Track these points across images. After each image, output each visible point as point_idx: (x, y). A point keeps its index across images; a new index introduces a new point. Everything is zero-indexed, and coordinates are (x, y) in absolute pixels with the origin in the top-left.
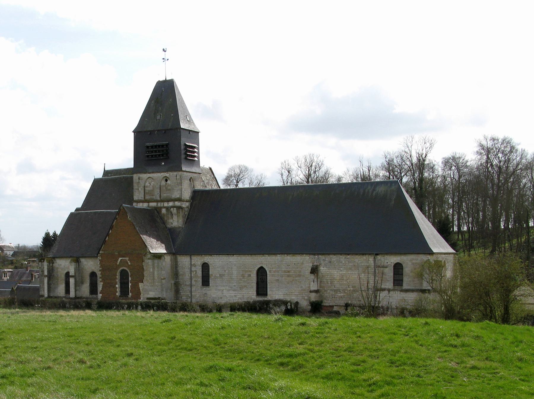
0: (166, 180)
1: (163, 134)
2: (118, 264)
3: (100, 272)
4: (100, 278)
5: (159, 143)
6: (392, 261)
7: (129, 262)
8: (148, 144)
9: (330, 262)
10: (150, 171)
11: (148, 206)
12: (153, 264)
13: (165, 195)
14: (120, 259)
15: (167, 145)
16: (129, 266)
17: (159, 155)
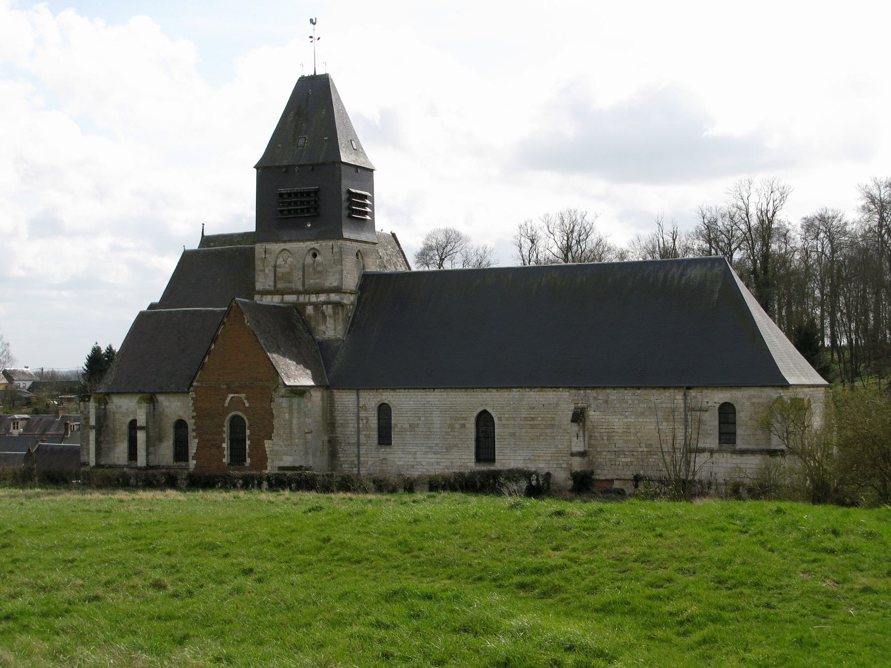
0: (315, 256)
1: (309, 169)
2: (226, 405)
7: (246, 401)
8: (282, 190)
9: (607, 402)
10: (285, 238)
11: (282, 302)
12: (290, 406)
13: (311, 281)
14: (230, 396)
15: (316, 192)
16: (245, 410)
17: (302, 210)
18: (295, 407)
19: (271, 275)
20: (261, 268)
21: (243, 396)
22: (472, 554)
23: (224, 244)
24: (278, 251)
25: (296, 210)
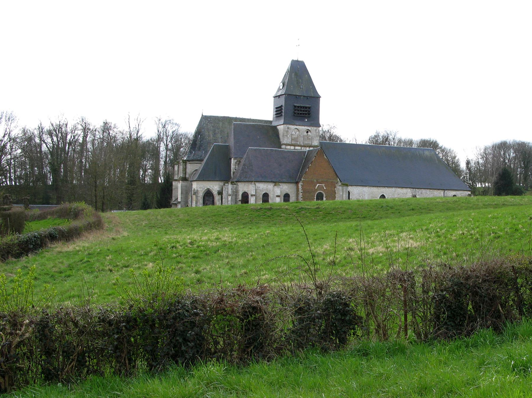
0: (307, 132)
1: (299, 99)
5: (304, 105)
8: (295, 105)
11: (295, 149)
12: (343, 190)
14: (318, 185)
15: (309, 108)
19: (290, 138)
25: (301, 114)
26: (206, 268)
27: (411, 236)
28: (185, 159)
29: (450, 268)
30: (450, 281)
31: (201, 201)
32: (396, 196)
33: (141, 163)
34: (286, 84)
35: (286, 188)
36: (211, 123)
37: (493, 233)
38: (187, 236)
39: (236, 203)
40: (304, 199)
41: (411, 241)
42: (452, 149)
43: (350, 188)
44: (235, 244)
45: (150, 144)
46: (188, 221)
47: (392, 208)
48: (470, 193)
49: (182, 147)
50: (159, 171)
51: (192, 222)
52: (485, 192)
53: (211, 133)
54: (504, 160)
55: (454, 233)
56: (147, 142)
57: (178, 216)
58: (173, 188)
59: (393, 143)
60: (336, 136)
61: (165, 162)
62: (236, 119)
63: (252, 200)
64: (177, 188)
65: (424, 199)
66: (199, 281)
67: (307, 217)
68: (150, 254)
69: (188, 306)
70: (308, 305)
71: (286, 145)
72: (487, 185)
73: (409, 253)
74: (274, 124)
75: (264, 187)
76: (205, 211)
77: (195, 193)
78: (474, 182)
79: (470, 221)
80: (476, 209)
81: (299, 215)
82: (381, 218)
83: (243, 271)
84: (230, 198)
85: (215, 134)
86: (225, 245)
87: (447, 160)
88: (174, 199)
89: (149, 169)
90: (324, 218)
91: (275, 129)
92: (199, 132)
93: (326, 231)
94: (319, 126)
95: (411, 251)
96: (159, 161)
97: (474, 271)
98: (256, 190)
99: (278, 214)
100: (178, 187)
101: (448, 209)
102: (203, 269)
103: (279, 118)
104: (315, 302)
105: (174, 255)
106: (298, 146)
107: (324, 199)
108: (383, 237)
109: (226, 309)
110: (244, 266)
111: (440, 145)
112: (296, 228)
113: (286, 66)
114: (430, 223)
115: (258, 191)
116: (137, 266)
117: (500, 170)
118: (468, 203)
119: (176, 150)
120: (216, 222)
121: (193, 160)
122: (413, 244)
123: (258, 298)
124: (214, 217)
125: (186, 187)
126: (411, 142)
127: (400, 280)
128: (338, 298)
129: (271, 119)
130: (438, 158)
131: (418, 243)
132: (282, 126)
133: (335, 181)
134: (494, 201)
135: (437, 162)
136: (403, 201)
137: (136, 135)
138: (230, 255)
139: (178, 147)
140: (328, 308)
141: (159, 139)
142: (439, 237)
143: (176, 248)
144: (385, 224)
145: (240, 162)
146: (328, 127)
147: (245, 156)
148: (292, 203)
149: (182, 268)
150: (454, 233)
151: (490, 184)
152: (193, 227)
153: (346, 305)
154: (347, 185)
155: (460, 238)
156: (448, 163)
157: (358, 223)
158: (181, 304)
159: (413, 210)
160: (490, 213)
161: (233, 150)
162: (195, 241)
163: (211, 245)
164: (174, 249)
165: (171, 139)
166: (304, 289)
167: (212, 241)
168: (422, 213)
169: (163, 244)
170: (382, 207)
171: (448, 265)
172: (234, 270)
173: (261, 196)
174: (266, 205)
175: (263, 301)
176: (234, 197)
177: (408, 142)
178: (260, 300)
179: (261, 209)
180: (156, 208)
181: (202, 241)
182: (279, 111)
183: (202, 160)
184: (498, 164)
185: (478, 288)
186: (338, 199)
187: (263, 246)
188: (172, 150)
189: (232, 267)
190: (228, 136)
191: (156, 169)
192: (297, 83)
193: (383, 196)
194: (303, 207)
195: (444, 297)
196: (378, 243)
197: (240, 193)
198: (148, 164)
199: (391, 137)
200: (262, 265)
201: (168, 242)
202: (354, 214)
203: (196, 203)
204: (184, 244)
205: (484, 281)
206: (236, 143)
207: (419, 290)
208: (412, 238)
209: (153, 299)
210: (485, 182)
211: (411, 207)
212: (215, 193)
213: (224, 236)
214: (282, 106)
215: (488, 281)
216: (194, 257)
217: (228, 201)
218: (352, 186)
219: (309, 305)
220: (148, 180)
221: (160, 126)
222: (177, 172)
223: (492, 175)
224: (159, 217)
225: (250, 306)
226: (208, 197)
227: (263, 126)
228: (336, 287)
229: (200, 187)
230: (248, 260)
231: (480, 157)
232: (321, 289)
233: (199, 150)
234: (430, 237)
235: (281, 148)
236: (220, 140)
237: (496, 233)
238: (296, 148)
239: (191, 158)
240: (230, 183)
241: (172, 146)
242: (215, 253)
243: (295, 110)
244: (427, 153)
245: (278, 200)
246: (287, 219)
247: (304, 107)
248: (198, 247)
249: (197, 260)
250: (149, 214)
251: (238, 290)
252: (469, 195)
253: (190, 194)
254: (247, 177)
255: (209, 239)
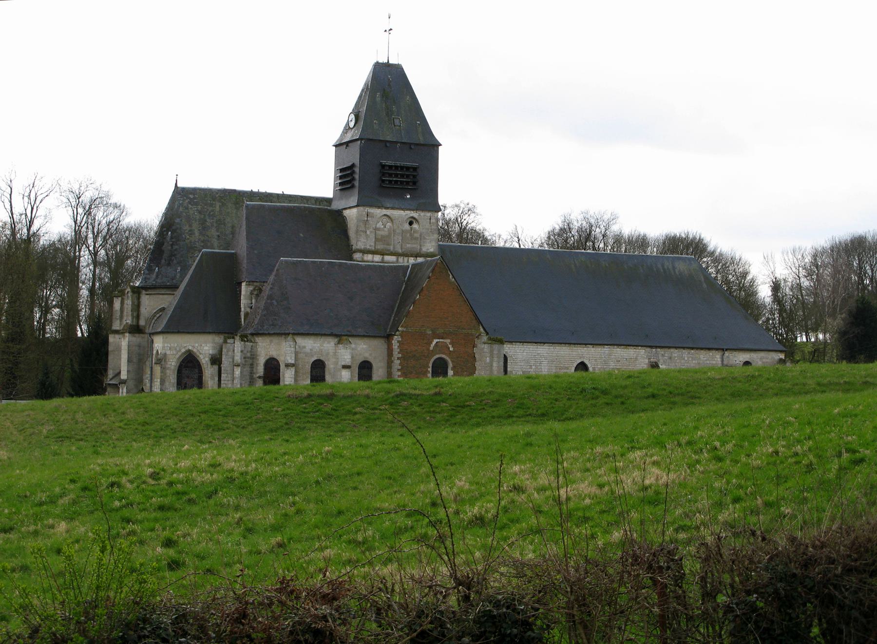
0: (411, 223)
1: (391, 145)
2: (431, 348)
3: (399, 362)
4: (398, 370)
5: (403, 164)
6: (741, 359)
7: (450, 346)
9: (670, 358)
10: (388, 206)
12: (491, 352)
13: (408, 246)
14: (435, 341)
15: (415, 169)
16: (450, 354)
17: (407, 183)
18: (495, 352)
20: (363, 229)
21: (448, 341)
22: (781, 466)
23: (290, 202)
24: (379, 216)
25: (396, 182)
26: (195, 534)
27: (655, 458)
28: (137, 284)
29: (764, 539)
30: (766, 569)
31: (172, 378)
32: (612, 365)
33: (36, 292)
34: (362, 115)
35: (363, 348)
36: (196, 204)
37: (847, 451)
38: (141, 460)
39: (252, 382)
40: (406, 372)
41: (655, 470)
42: (737, 257)
43: (509, 349)
44: (254, 478)
45: (57, 250)
46: (145, 423)
47: (605, 392)
48: (782, 356)
49: (129, 257)
50: (78, 311)
51: (154, 428)
52: (817, 354)
53: (196, 226)
54: (861, 280)
55: (754, 451)
56: (50, 245)
57: (123, 413)
58: (110, 348)
59: (602, 245)
60: (473, 231)
61: (92, 291)
62: (252, 195)
63: (288, 377)
64: (119, 349)
65: (679, 371)
66: (174, 565)
67: (414, 414)
68: (61, 502)
69: (166, 630)
70: (441, 626)
71: (365, 252)
72: (821, 336)
73: (654, 498)
74: (336, 206)
75: (314, 347)
76: (182, 402)
77: (159, 361)
78: (790, 330)
79: (788, 423)
80: (800, 393)
81: (400, 409)
82: (582, 416)
83: (273, 541)
84: (238, 372)
85: (204, 229)
86: (232, 480)
87: (727, 282)
88: (111, 373)
89: (55, 307)
90: (451, 416)
91: (338, 217)
92: (169, 222)
93: (459, 446)
94: (437, 209)
95: (657, 493)
96: (78, 289)
97: (823, 545)
98: (296, 353)
99: (348, 407)
100: (121, 347)
101: (736, 395)
102: (184, 536)
103: (347, 193)
104: (455, 618)
105: (117, 504)
106: (392, 254)
107: (450, 372)
108: (589, 460)
109: (254, 636)
110: (276, 528)
111: (711, 248)
112: (391, 440)
113: (358, 79)
114: (696, 428)
115: (301, 356)
116: (32, 528)
117: (852, 304)
118: (780, 381)
119: (115, 265)
120: (208, 426)
121: (154, 288)
122: (655, 477)
123: (325, 609)
124: (203, 416)
125: (139, 346)
126: (642, 242)
127: (650, 567)
128: (508, 608)
129: (329, 194)
130: (707, 276)
131: (672, 476)
132: (355, 210)
133: (473, 332)
134: (842, 376)
135: (705, 286)
136: (629, 377)
137: (25, 230)
138: (243, 503)
139: (121, 259)
140: (485, 632)
141: (78, 239)
142: (720, 459)
143: (119, 485)
144: (593, 432)
145: (260, 290)
146: (456, 209)
147: (272, 278)
148: (379, 383)
149: (133, 533)
150: (754, 451)
151: (828, 335)
152: (158, 439)
153: (527, 625)
154: (501, 342)
155: (768, 464)
156: (729, 288)
157: (528, 428)
158: (150, 623)
159: (654, 396)
160: (837, 404)
161: (244, 264)
162: (163, 470)
163: (199, 479)
164: (116, 489)
165: (105, 239)
166: (430, 587)
167: (201, 471)
168: (674, 403)
169: (91, 479)
170: (583, 390)
171: (758, 533)
172: (254, 538)
173: (308, 367)
174: (320, 389)
175: (337, 615)
176: (247, 369)
177: (637, 241)
178: (331, 614)
179: (309, 396)
180: (72, 396)
181: (179, 471)
182: (346, 178)
183: (175, 287)
184: (846, 288)
185: (835, 587)
186: (481, 372)
187: (317, 482)
188: (107, 263)
189: (250, 530)
190: (233, 233)
191: (70, 307)
192: (387, 114)
193: (582, 366)
194: (406, 391)
195: (754, 608)
196: (579, 475)
197: (262, 361)
198: (53, 295)
199: (597, 232)
200: (316, 526)
201: (101, 474)
202: (521, 406)
203: (162, 383)
204: (139, 477)
205: (848, 570)
206: (250, 248)
207: (694, 592)
208: (654, 463)
209: (86, 613)
210: (815, 330)
211: (650, 390)
212: (204, 360)
213: (228, 459)
214: (353, 165)
215: (856, 569)
216: (161, 508)
217: (234, 379)
218: (511, 342)
219: (442, 625)
220: (51, 331)
221: (80, 210)
222: (119, 314)
223: (833, 315)
224: (79, 416)
225: (308, 629)
226: (189, 370)
227: (311, 211)
228: (501, 582)
229: (168, 347)
230: (286, 515)
231: (803, 273)
232: (469, 589)
233: (169, 265)
234: (698, 462)
235: (351, 259)
236: (216, 243)
237: (854, 452)
238: (387, 258)
239: (151, 282)
240: (237, 338)
241: (107, 254)
242: (210, 497)
243: (384, 174)
244: (681, 267)
245: (346, 375)
246: (368, 420)
247: (402, 168)
248: (171, 484)
249: (169, 514)
250: (57, 408)
251: (280, 591)
252: (781, 361)
253: (148, 363)
254: (274, 325)
255: (195, 467)
